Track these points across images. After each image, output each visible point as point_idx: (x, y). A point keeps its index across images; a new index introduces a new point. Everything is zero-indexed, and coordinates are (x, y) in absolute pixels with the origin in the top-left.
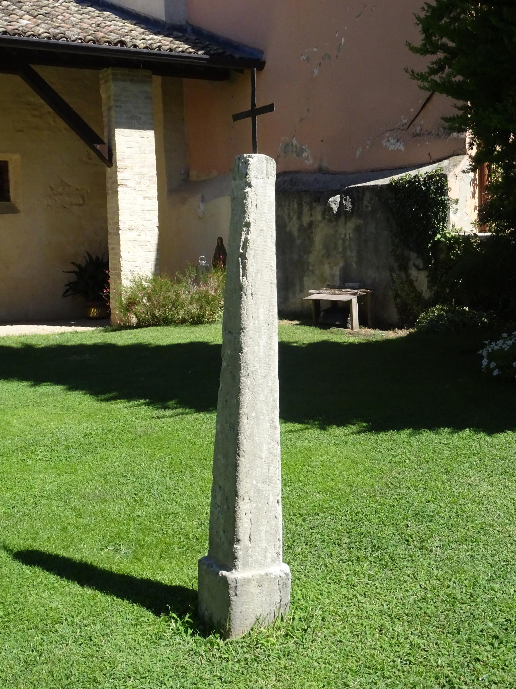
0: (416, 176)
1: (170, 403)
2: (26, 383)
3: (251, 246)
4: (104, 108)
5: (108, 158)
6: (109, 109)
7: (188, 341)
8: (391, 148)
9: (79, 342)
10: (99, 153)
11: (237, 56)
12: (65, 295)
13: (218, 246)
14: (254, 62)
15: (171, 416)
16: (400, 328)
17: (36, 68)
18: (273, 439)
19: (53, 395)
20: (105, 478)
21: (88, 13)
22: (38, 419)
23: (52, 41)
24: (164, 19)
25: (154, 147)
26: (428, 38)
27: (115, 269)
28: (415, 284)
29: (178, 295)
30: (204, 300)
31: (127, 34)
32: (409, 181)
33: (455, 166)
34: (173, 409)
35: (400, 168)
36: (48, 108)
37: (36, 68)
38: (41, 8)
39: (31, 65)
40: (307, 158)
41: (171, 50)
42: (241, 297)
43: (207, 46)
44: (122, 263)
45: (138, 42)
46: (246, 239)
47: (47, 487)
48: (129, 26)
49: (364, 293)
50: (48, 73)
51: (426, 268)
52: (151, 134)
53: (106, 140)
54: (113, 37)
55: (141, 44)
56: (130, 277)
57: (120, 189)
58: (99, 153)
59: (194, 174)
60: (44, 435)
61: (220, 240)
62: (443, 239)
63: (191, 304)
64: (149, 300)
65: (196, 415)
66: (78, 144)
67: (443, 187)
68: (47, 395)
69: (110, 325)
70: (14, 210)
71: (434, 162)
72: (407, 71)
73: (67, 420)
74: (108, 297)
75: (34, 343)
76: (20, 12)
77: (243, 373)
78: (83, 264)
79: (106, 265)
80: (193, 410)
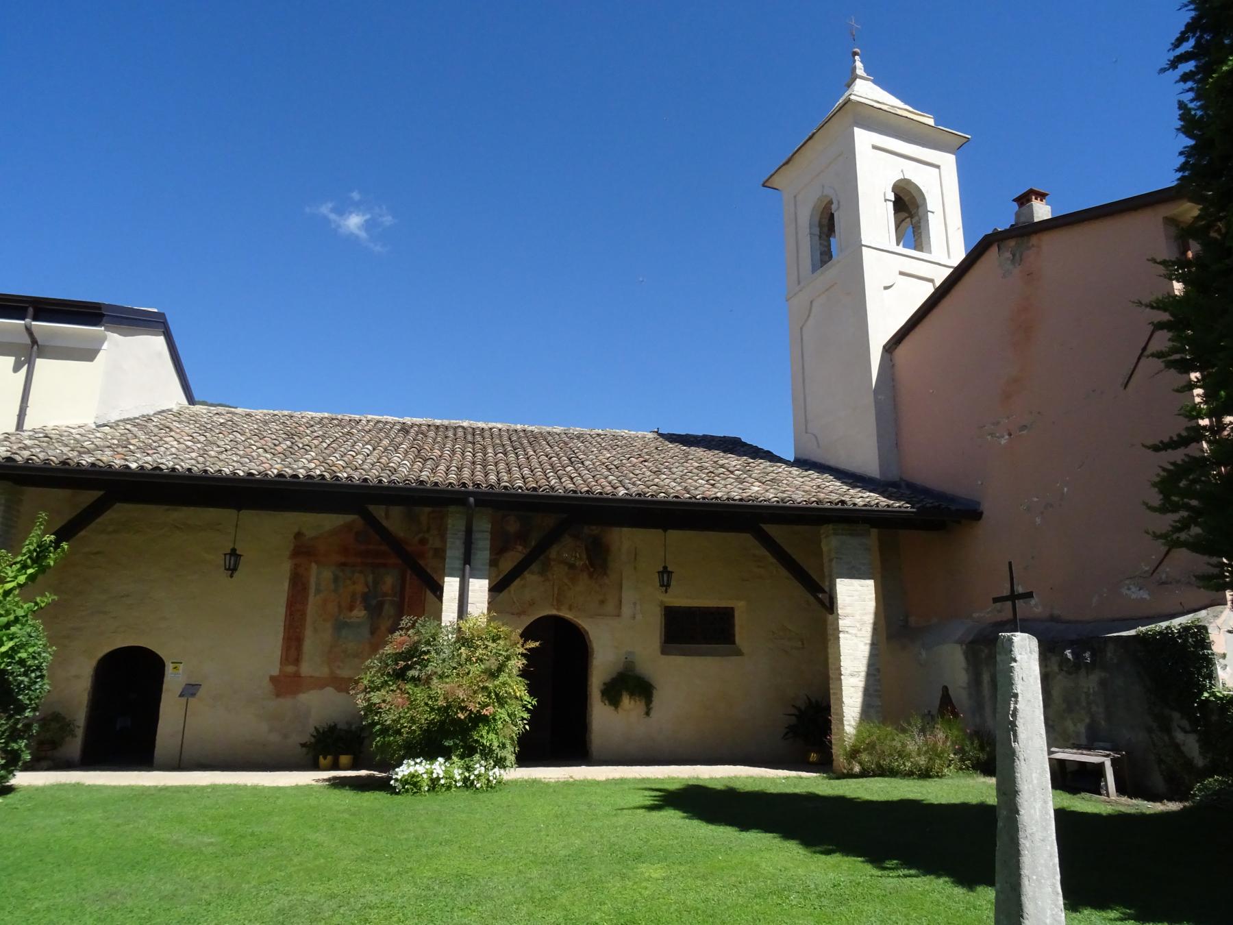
0: (1168, 627)
3: (1020, 715)
4: (826, 560)
5: (830, 605)
6: (831, 560)
8: (1134, 596)
14: (972, 513)
16: (1170, 800)
17: (764, 527)
18: (1056, 906)
24: (878, 477)
26: (1166, 497)
28: (1183, 748)
29: (904, 745)
32: (1160, 633)
33: (1216, 616)
35: (1148, 618)
36: (772, 560)
37: (764, 527)
40: (1036, 605)
42: (1013, 761)
44: (845, 709)
45: (858, 501)
46: (1015, 710)
50: (772, 529)
51: (1194, 731)
52: (871, 583)
53: (827, 589)
54: (834, 497)
55: (860, 502)
57: (841, 635)
61: (945, 689)
62: (1212, 699)
63: (919, 755)
66: (798, 591)
67: (1203, 640)
70: (739, 653)
71: (1189, 612)
72: (1147, 533)
74: (830, 742)
76: (751, 480)
77: (1021, 834)
79: (828, 708)
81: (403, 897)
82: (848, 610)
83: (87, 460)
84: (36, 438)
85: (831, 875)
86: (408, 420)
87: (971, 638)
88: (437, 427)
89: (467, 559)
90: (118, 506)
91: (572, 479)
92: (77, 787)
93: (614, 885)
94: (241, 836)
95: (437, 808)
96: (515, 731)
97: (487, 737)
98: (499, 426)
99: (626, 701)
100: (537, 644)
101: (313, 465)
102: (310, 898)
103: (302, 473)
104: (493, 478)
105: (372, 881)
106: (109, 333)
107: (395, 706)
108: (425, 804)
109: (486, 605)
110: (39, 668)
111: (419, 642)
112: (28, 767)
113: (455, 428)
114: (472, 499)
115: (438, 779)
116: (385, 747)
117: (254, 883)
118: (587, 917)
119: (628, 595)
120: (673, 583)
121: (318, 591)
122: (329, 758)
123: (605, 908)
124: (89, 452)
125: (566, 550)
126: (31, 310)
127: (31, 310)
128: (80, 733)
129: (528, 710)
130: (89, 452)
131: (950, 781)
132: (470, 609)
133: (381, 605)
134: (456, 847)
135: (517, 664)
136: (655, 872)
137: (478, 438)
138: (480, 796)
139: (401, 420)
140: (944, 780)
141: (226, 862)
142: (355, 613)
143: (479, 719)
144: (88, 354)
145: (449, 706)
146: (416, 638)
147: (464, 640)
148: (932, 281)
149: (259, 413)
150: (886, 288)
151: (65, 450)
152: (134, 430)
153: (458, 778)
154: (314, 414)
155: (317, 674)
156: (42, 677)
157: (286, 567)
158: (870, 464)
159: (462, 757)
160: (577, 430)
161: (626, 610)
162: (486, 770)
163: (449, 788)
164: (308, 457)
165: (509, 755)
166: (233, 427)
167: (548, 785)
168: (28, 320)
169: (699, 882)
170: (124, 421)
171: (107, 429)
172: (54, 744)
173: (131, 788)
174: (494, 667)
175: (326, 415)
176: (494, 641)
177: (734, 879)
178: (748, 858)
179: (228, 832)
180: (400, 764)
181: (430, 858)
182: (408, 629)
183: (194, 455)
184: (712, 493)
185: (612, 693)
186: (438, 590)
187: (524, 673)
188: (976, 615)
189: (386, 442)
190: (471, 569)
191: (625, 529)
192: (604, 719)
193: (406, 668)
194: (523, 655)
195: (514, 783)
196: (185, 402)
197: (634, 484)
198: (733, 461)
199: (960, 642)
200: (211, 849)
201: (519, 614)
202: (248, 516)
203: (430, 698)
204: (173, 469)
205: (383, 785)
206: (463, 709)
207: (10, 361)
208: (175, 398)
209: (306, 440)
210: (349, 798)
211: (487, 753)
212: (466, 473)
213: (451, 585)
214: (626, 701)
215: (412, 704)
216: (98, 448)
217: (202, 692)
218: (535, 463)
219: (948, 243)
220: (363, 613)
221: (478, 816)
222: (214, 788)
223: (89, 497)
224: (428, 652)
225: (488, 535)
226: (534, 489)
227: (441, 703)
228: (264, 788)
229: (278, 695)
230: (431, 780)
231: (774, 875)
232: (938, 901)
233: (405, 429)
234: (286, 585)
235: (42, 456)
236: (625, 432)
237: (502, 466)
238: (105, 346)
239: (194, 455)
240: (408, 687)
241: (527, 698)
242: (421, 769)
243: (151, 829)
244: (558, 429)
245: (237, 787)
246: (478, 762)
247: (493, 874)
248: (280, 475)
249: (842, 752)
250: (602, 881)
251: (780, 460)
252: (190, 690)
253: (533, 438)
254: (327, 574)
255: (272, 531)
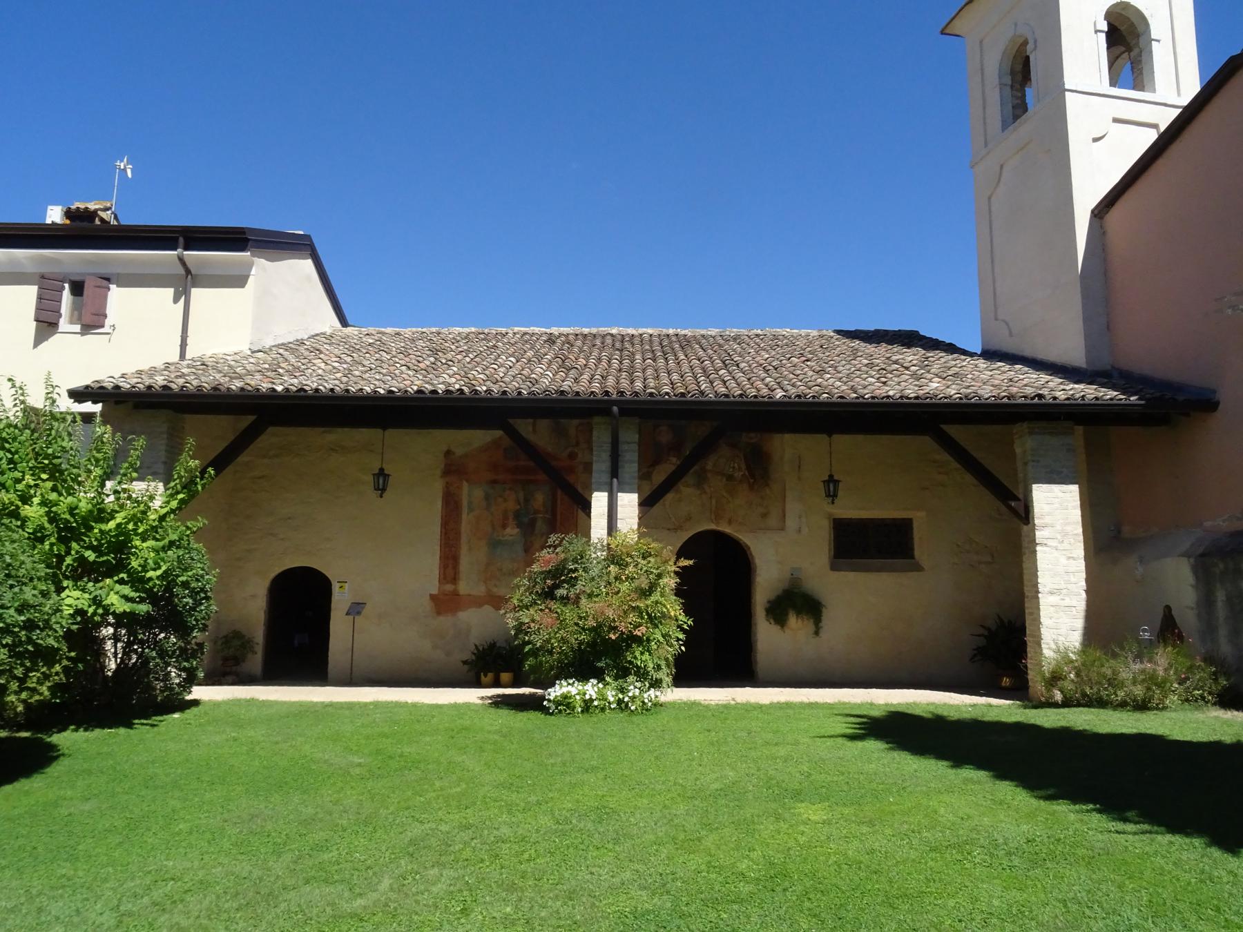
1: (1129, 814)
2: (945, 763)
4: (1019, 464)
5: (1025, 514)
6: (1026, 464)
7: (1135, 731)
9: (996, 719)
10: (1014, 511)
11: (1181, 398)
12: (972, 659)
13: (1165, 615)
15: (1135, 833)
17: (944, 427)
19: (979, 782)
20: (1065, 906)
21: (997, 369)
22: (967, 810)
23: (965, 401)
24: (1084, 366)
25: (1079, 503)
27: (1034, 636)
29: (1115, 673)
30: (1151, 680)
31: (1043, 386)
34: (1136, 823)
36: (954, 464)
38: (949, 368)
39: (943, 426)
41: (1097, 398)
43: (1141, 390)
45: (1058, 394)
47: (996, 903)
48: (1044, 377)
49: (1220, 596)
50: (952, 430)
52: (1075, 488)
53: (1021, 496)
54: (1029, 391)
55: (1061, 395)
56: (1054, 647)
57: (1038, 548)
58: (1014, 511)
59: (1126, 531)
60: (978, 833)
64: (1077, 675)
65: (1169, 837)
68: (971, 781)
69: (1029, 700)
70: (918, 568)
73: (1002, 817)
74: (1026, 667)
75: (945, 714)
76: (929, 376)
78: (993, 628)
79: (1022, 630)
80: (1163, 829)
81: (538, 831)
82: (1047, 520)
83: (237, 385)
84: (193, 367)
85: (1025, 827)
86: (555, 331)
87: (1201, 550)
88: (585, 336)
89: (614, 473)
90: (271, 429)
91: (725, 382)
92: (251, 702)
93: (767, 828)
94: (390, 757)
95: (589, 730)
96: (670, 651)
97: (640, 657)
98: (650, 331)
99: (793, 620)
100: (691, 562)
101: (453, 380)
102: (444, 828)
103: (441, 388)
104: (639, 385)
105: (510, 812)
106: (256, 259)
107: (546, 627)
108: (581, 725)
109: (636, 520)
110: (202, 590)
111: (565, 559)
112: (214, 679)
113: (604, 337)
114: (615, 409)
115: (591, 700)
116: (536, 669)
117: (392, 809)
118: (733, 865)
119: (793, 508)
120: (840, 493)
121: (471, 510)
122: (490, 675)
123: (754, 855)
124: (240, 377)
125: (724, 459)
126: (181, 240)
127: (181, 240)
128: (260, 650)
129: (682, 630)
130: (240, 377)
131: (1173, 715)
132: (620, 525)
133: (532, 523)
134: (601, 775)
135: (670, 582)
136: (814, 813)
137: (627, 345)
138: (635, 719)
139: (548, 331)
140: (1166, 714)
141: (370, 784)
142: (509, 530)
143: (633, 639)
144: (238, 280)
145: (600, 626)
146: (563, 556)
147: (615, 558)
148: (1155, 126)
149: (407, 332)
150: (1096, 140)
151: (218, 376)
152: (286, 354)
153: (612, 699)
154: (461, 330)
155: (474, 593)
156: (207, 598)
157: (438, 486)
158: (1076, 355)
159: (616, 679)
160: (734, 331)
161: (791, 522)
162: (641, 691)
163: (603, 710)
164: (451, 372)
165: (665, 676)
166: (381, 346)
167: (707, 707)
168: (180, 250)
169: (865, 829)
170: (278, 346)
171: (260, 355)
172: (237, 660)
173: (300, 704)
174: (645, 586)
175: (473, 329)
176: (644, 558)
177: (906, 826)
178: (924, 802)
179: (378, 752)
180: (553, 685)
181: (573, 786)
182: (555, 547)
183: (338, 375)
184: (882, 391)
185: (779, 610)
186: (586, 507)
187: (678, 592)
188: (1208, 524)
189: (530, 354)
190: (619, 483)
191: (787, 436)
192: (769, 639)
193: (556, 584)
194: (676, 573)
195: (673, 705)
196: (337, 324)
197: (793, 385)
198: (911, 356)
199: (1186, 555)
200: (358, 771)
201: (676, 530)
202: (393, 435)
203: (580, 618)
204: (317, 390)
205: (534, 704)
206: (615, 628)
207: (170, 292)
208: (327, 321)
209: (449, 356)
210: (506, 717)
211: (642, 674)
212: (611, 381)
213: (599, 501)
214: (793, 620)
215: (562, 624)
216: (249, 373)
217: (367, 611)
218: (685, 368)
219: (1177, 74)
220: (516, 531)
221: (629, 741)
222: (376, 705)
223: (248, 420)
224: (576, 570)
225: (635, 447)
226: (683, 395)
227: (591, 623)
228: (423, 705)
229: (439, 613)
230: (585, 701)
231: (953, 824)
232: (1162, 868)
233: (551, 340)
234: (439, 504)
235: (195, 383)
236: (786, 331)
237: (649, 372)
238: (253, 272)
239: (338, 375)
240: (554, 605)
241: (682, 618)
242: (573, 691)
243: (307, 747)
244: (713, 332)
245: (398, 705)
246: (633, 683)
247: (636, 807)
248: (419, 391)
249: (1039, 678)
250: (753, 822)
251: (964, 352)
252: (356, 609)
253: (685, 342)
254: (479, 493)
255: (424, 448)
